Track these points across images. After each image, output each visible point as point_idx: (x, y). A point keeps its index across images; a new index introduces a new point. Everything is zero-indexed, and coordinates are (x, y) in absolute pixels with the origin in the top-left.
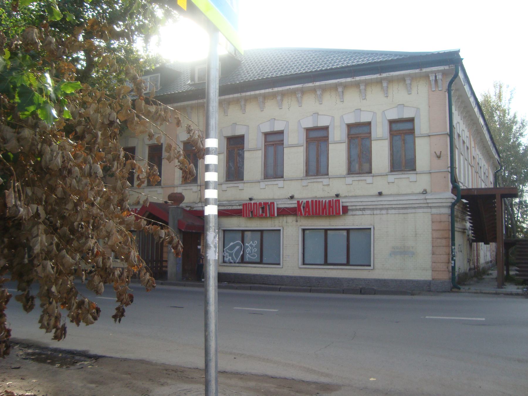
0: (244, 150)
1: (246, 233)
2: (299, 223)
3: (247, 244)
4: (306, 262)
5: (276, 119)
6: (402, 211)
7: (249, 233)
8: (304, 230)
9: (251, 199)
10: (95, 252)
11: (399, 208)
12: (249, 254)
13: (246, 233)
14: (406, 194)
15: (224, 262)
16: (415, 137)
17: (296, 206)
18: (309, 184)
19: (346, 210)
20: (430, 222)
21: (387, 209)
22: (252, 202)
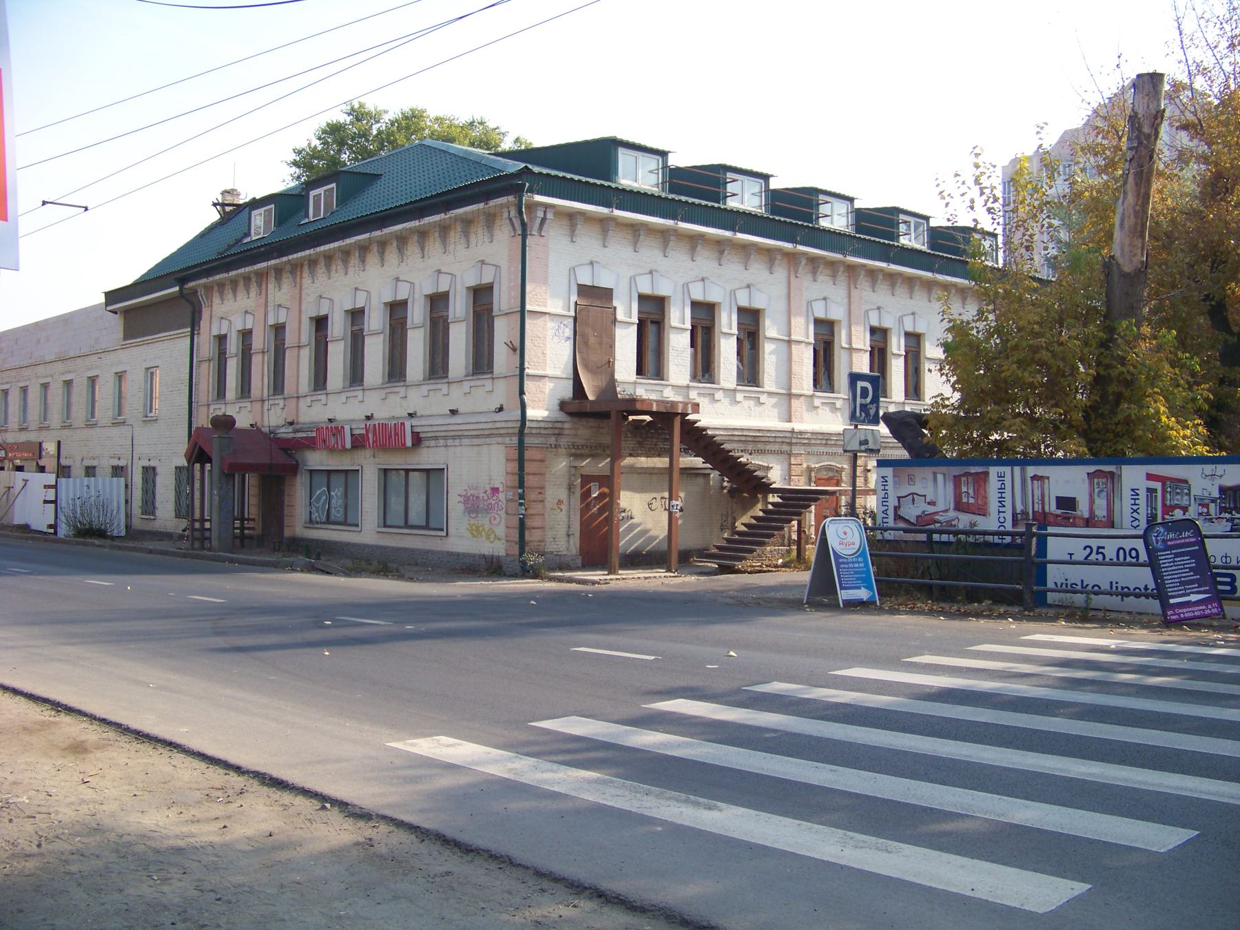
0: (449, 321)
1: (411, 474)
2: (377, 460)
3: (332, 493)
4: (388, 523)
5: (401, 278)
6: (476, 441)
7: (416, 474)
8: (386, 472)
9: (330, 420)
10: (780, 501)
11: (477, 436)
12: (335, 508)
13: (411, 474)
14: (473, 413)
15: (311, 521)
16: (493, 317)
17: (363, 432)
18: (432, 393)
19: (418, 440)
20: (504, 460)
21: (446, 438)
22: (333, 425)
